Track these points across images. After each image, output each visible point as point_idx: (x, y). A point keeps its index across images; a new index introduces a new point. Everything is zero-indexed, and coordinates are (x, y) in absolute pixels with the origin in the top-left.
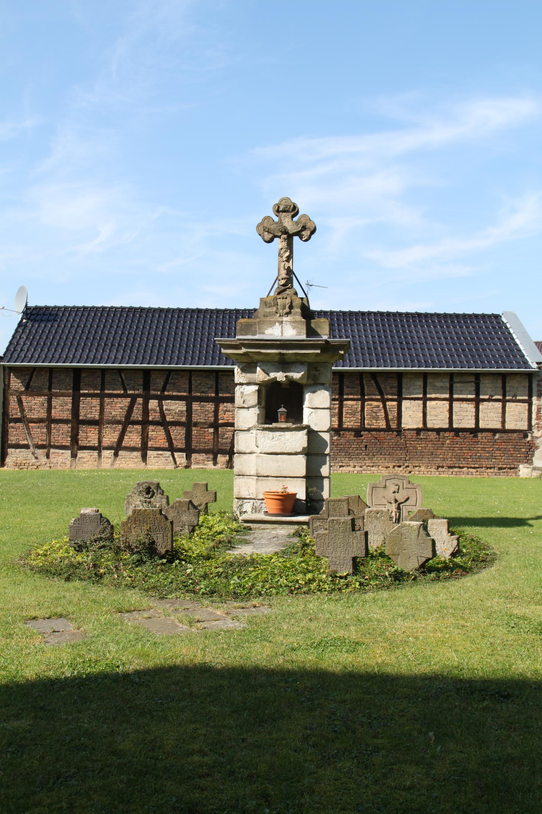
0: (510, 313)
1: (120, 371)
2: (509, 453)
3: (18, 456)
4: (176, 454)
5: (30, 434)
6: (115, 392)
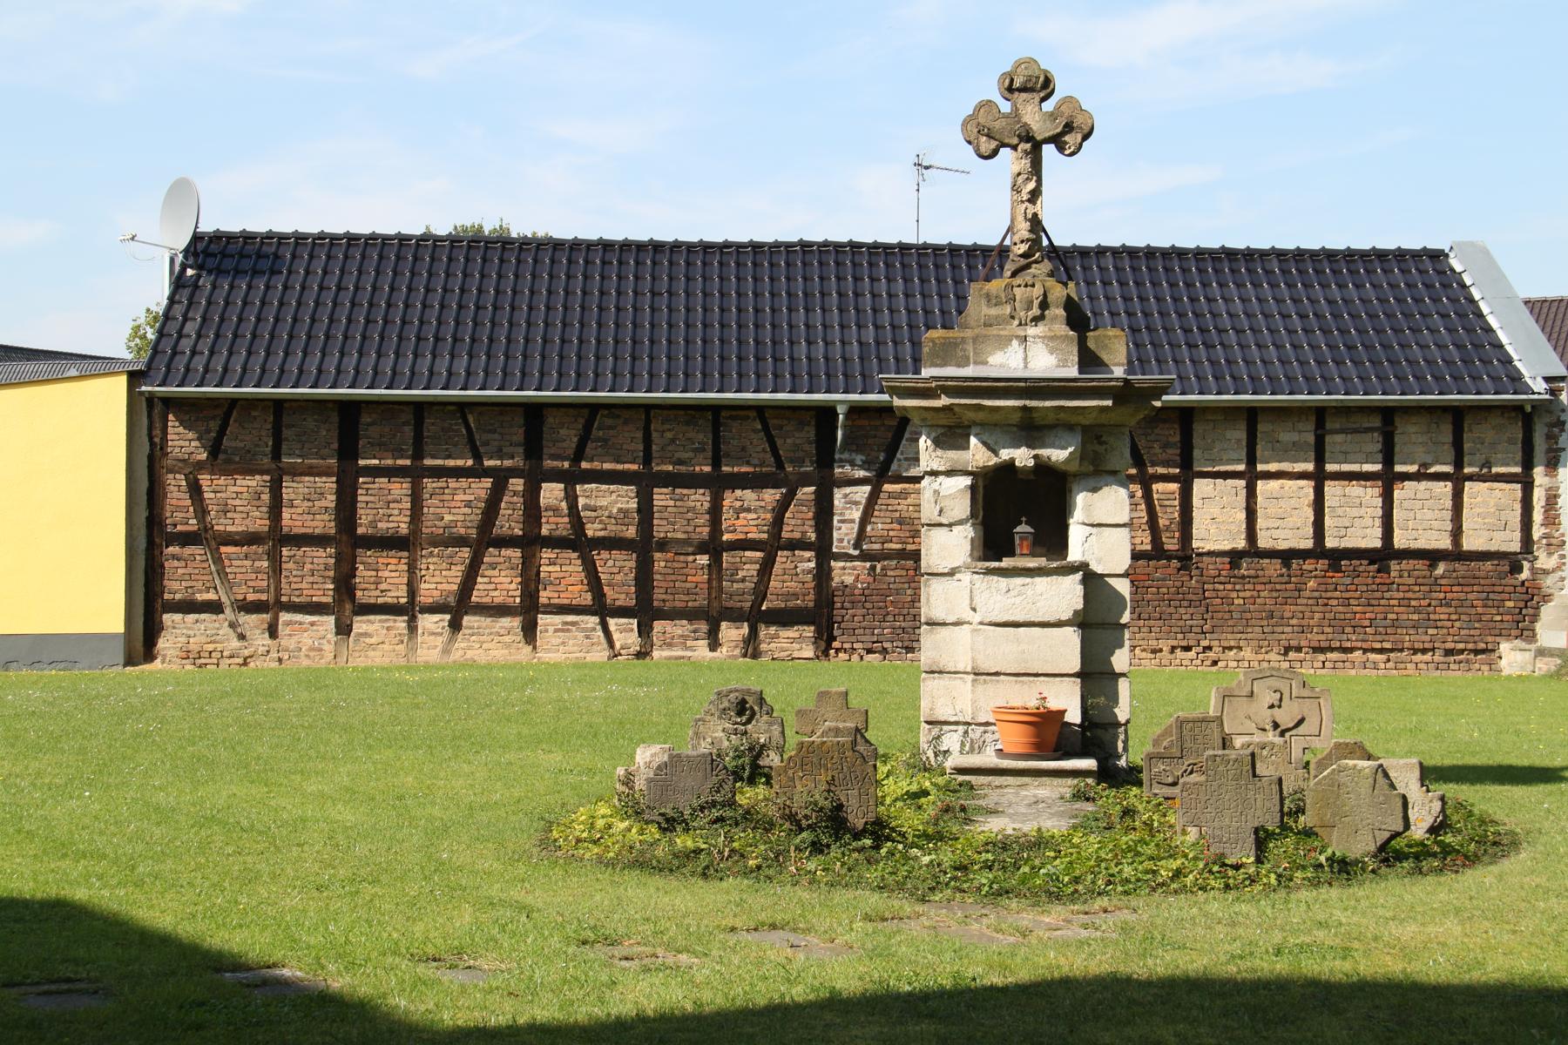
0: (1472, 244)
1: (462, 408)
2: (1473, 611)
3: (191, 633)
4: (612, 623)
5: (222, 573)
6: (451, 463)
